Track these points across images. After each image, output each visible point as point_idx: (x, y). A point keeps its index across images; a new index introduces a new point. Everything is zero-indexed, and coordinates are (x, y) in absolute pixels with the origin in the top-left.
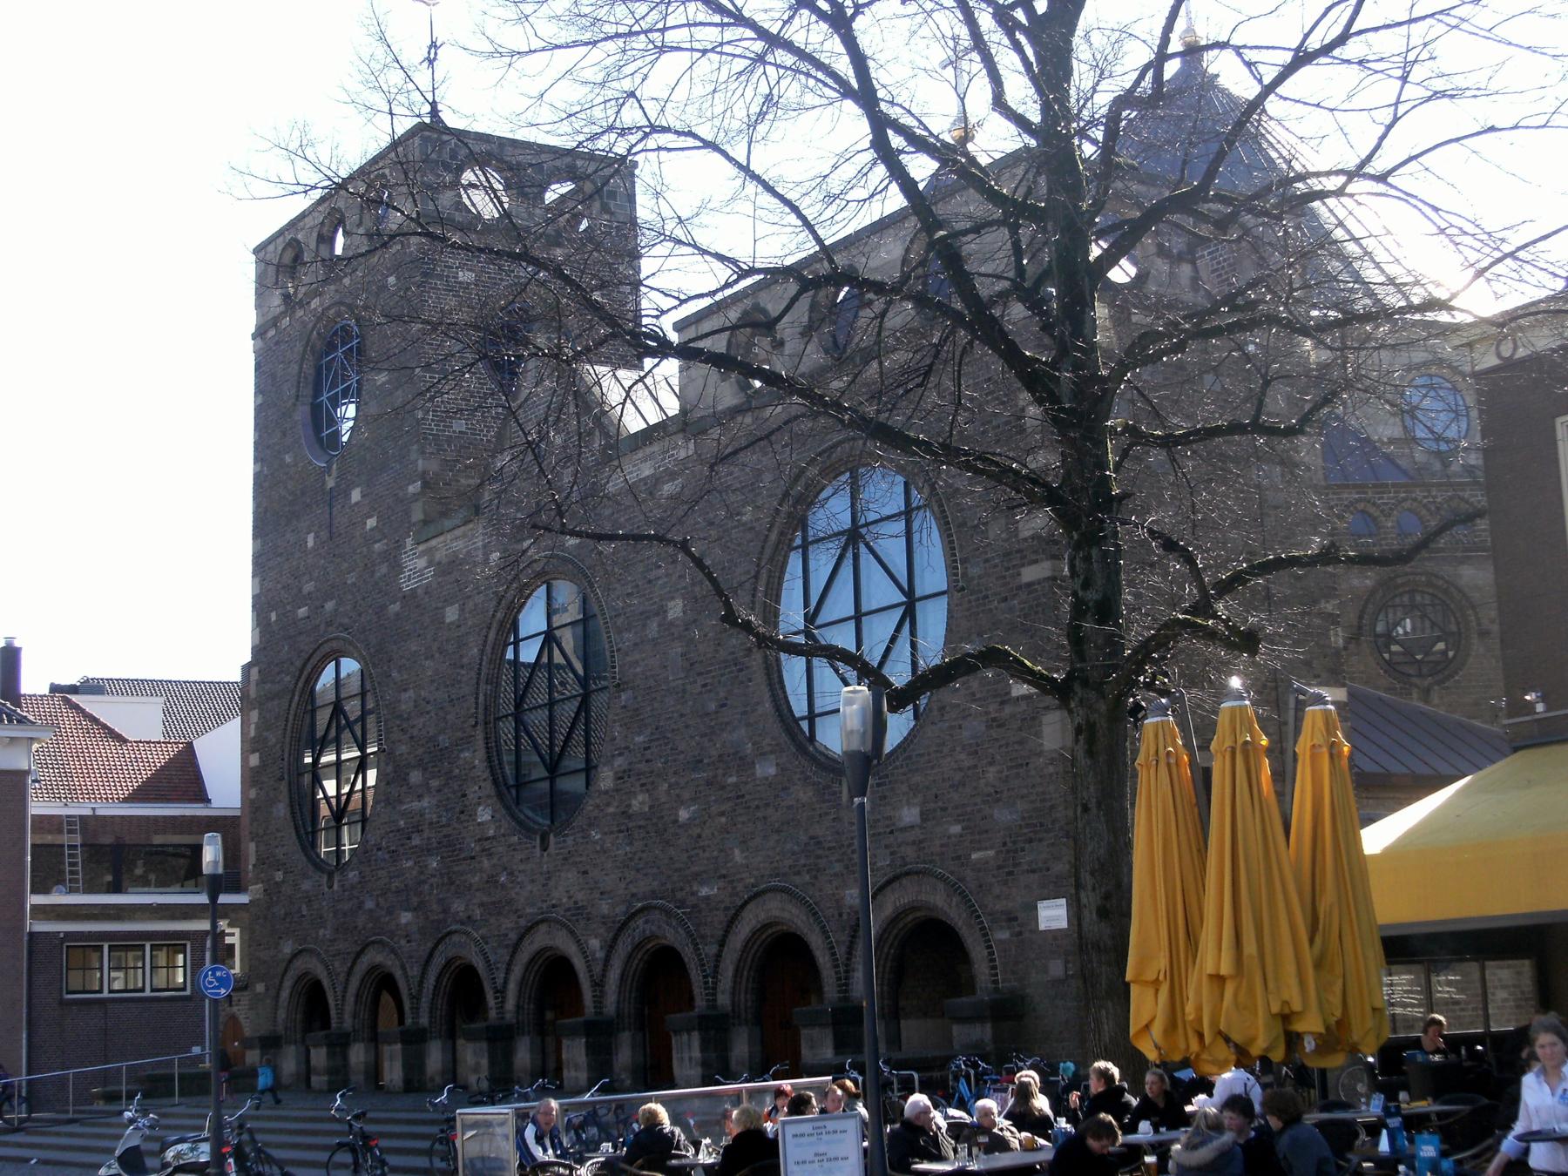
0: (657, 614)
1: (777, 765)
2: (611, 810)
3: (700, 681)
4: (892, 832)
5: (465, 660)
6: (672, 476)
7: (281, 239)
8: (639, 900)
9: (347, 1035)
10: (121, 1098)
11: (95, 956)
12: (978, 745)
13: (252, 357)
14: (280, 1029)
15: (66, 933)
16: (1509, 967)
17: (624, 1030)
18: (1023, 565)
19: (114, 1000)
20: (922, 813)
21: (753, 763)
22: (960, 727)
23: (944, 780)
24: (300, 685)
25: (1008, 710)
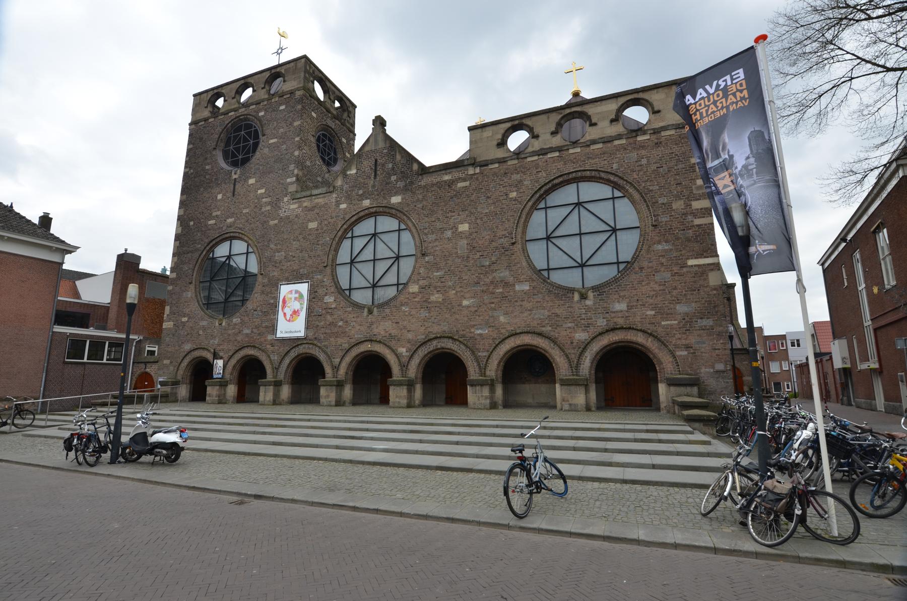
1: (530, 286)
4: (608, 313)
5: (320, 242)
7: (212, 92)
8: (433, 334)
10: (108, 405)
14: (179, 378)
15: (70, 333)
16: (590, 374)
17: (417, 383)
20: (628, 306)
21: (514, 285)
23: (642, 294)
24: (208, 248)
25: (685, 270)
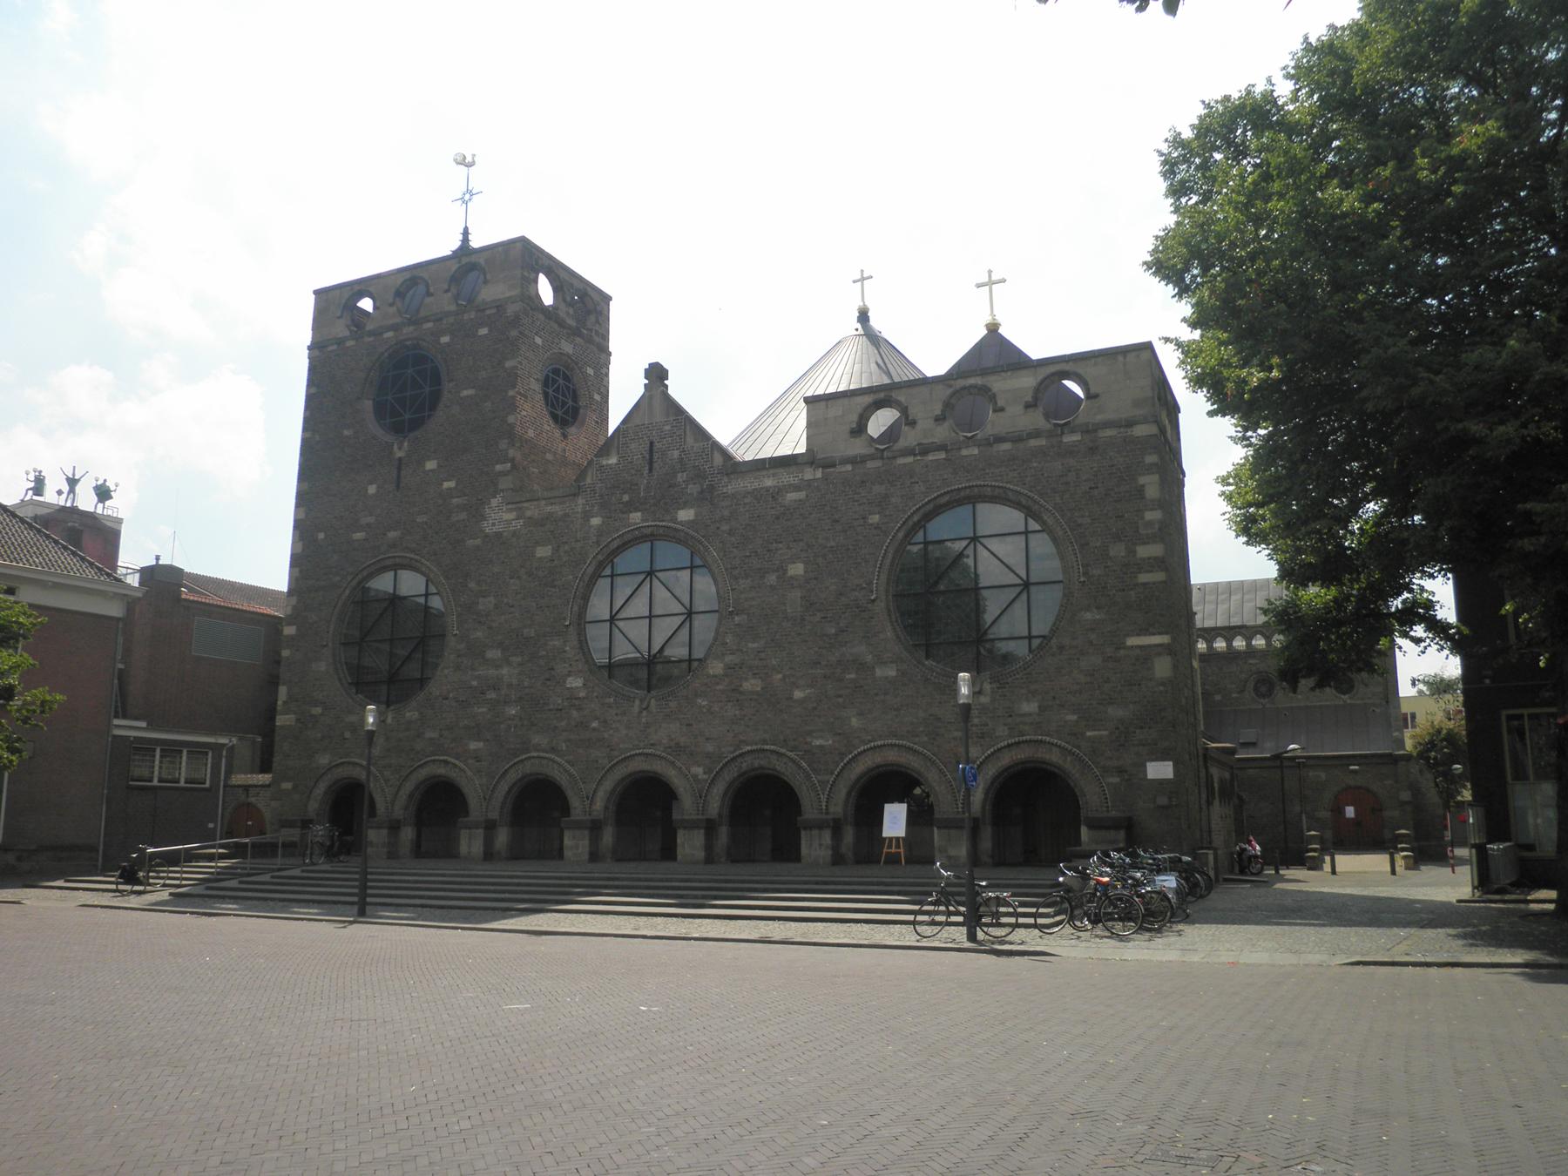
0: (777, 571)
2: (720, 687)
3: (819, 615)
4: (1011, 716)
6: (797, 488)
9: (399, 821)
11: (164, 776)
12: (1094, 670)
13: (307, 361)
18: (1140, 573)
19: (160, 788)
20: (1039, 707)
21: (873, 667)
22: (1078, 659)
